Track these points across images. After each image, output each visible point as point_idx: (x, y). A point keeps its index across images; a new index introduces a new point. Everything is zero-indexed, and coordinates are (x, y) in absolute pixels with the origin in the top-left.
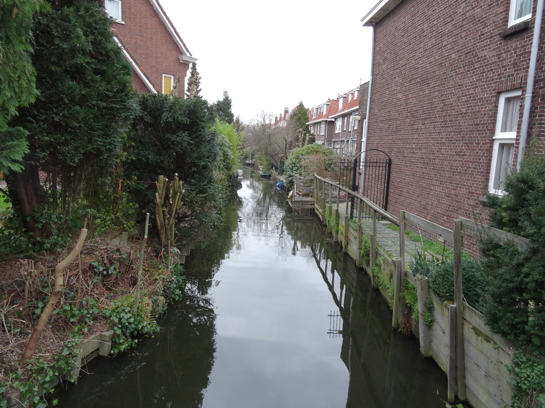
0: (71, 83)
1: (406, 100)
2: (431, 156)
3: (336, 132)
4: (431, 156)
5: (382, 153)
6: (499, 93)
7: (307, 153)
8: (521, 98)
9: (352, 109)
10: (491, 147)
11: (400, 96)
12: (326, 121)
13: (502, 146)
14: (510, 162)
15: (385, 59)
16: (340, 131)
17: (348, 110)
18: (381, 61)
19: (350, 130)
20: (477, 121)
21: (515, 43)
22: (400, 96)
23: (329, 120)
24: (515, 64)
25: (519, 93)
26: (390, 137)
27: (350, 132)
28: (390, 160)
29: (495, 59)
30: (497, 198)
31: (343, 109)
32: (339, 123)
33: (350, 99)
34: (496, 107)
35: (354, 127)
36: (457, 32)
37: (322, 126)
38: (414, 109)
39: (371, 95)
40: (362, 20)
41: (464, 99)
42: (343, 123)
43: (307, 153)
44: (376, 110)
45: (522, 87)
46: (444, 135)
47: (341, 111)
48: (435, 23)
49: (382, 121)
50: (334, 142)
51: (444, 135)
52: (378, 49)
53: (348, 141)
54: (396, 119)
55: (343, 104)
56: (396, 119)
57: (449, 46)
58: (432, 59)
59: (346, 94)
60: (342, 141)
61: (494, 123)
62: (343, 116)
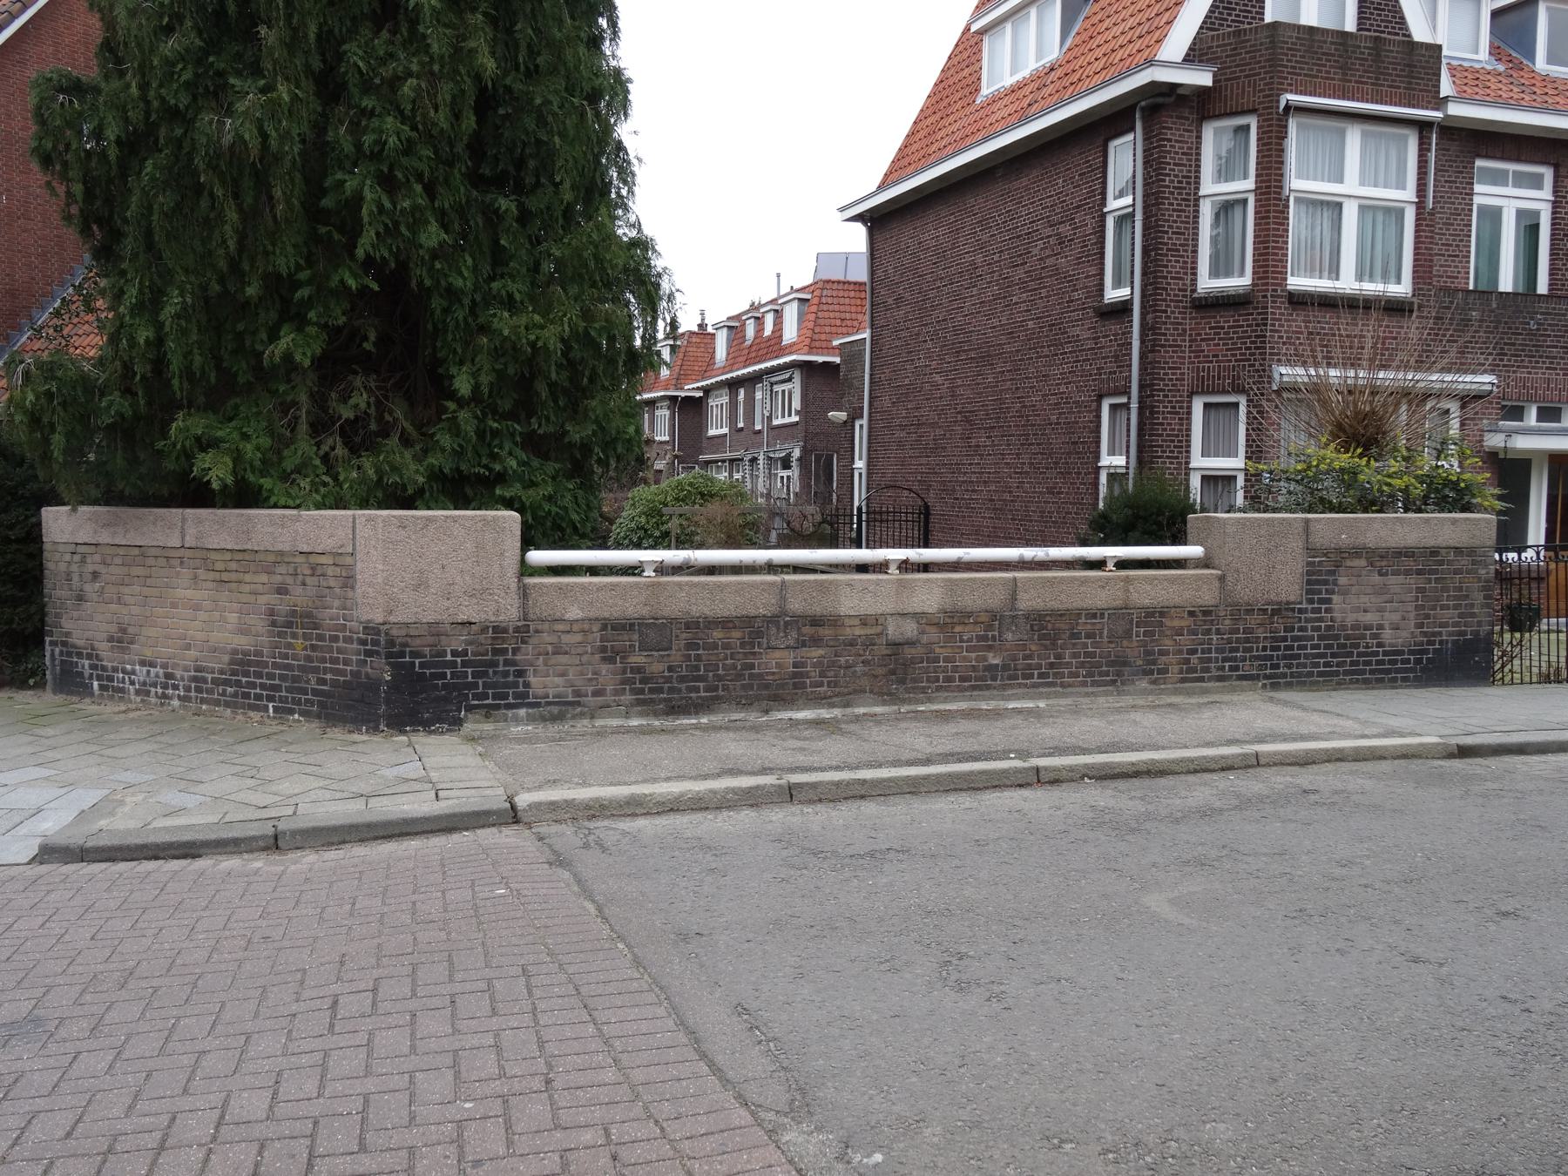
0: (303, 398)
1: (952, 389)
2: (1007, 496)
3: (712, 432)
4: (1007, 496)
5: (906, 493)
6: (1100, 397)
7: (677, 499)
8: (1126, 406)
9: (763, 366)
10: (1097, 478)
11: (938, 378)
12: (673, 399)
13: (1110, 475)
14: (123, 708)
15: (899, 300)
16: (725, 430)
17: (750, 369)
18: (890, 301)
19: (758, 427)
20: (1075, 438)
21: (1114, 327)
22: (938, 378)
23: (683, 394)
24: (1116, 357)
25: (1124, 400)
26: (924, 461)
27: (760, 432)
28: (927, 507)
29: (1091, 344)
30: (649, 291)
31: (732, 363)
32: (718, 402)
33: (750, 331)
34: (1099, 417)
35: (770, 418)
36: (1032, 285)
37: (658, 413)
38: (969, 407)
39: (872, 368)
40: (842, 209)
41: (1053, 400)
42: (733, 404)
43: (677, 499)
44: (886, 402)
45: (1126, 392)
46: (1025, 458)
47: (724, 370)
48: (996, 257)
49: (902, 427)
50: (707, 463)
51: (1025, 458)
52: (880, 273)
53: (754, 460)
54: (934, 425)
55: (729, 347)
56: (934, 425)
57: (1023, 307)
58: (995, 322)
59: (737, 317)
60: (732, 461)
61: (1098, 443)
62: (733, 385)
